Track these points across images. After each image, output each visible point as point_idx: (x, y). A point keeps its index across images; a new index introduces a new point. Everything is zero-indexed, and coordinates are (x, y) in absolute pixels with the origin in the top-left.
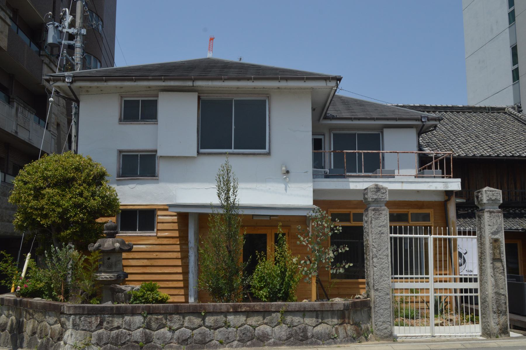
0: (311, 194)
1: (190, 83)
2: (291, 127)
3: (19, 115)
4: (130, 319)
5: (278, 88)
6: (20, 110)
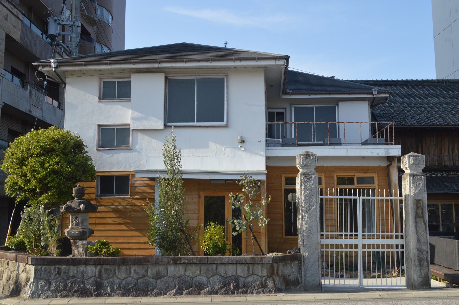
0: (264, 159)
1: (156, 65)
3: (33, 96)
4: (84, 269)
5: (235, 68)
6: (33, 93)
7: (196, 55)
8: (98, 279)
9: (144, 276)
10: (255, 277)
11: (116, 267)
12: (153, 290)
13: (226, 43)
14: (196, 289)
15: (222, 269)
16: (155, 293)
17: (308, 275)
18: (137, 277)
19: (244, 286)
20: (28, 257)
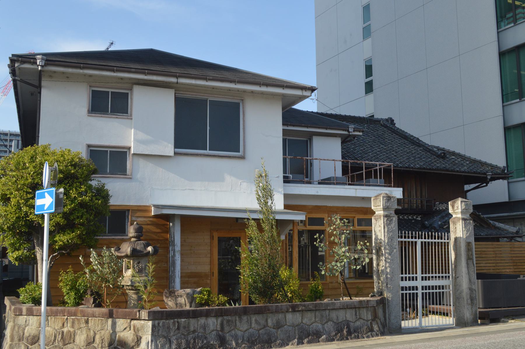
1: (174, 80)
2: (263, 130)
7: (211, 73)
8: (220, 333)
9: (265, 327)
10: (361, 321)
11: (237, 317)
12: (275, 341)
13: (112, 43)
14: (315, 337)
15: (334, 315)
16: (279, 344)
17: (392, 317)
18: (259, 328)
19: (355, 331)
20: (139, 311)
